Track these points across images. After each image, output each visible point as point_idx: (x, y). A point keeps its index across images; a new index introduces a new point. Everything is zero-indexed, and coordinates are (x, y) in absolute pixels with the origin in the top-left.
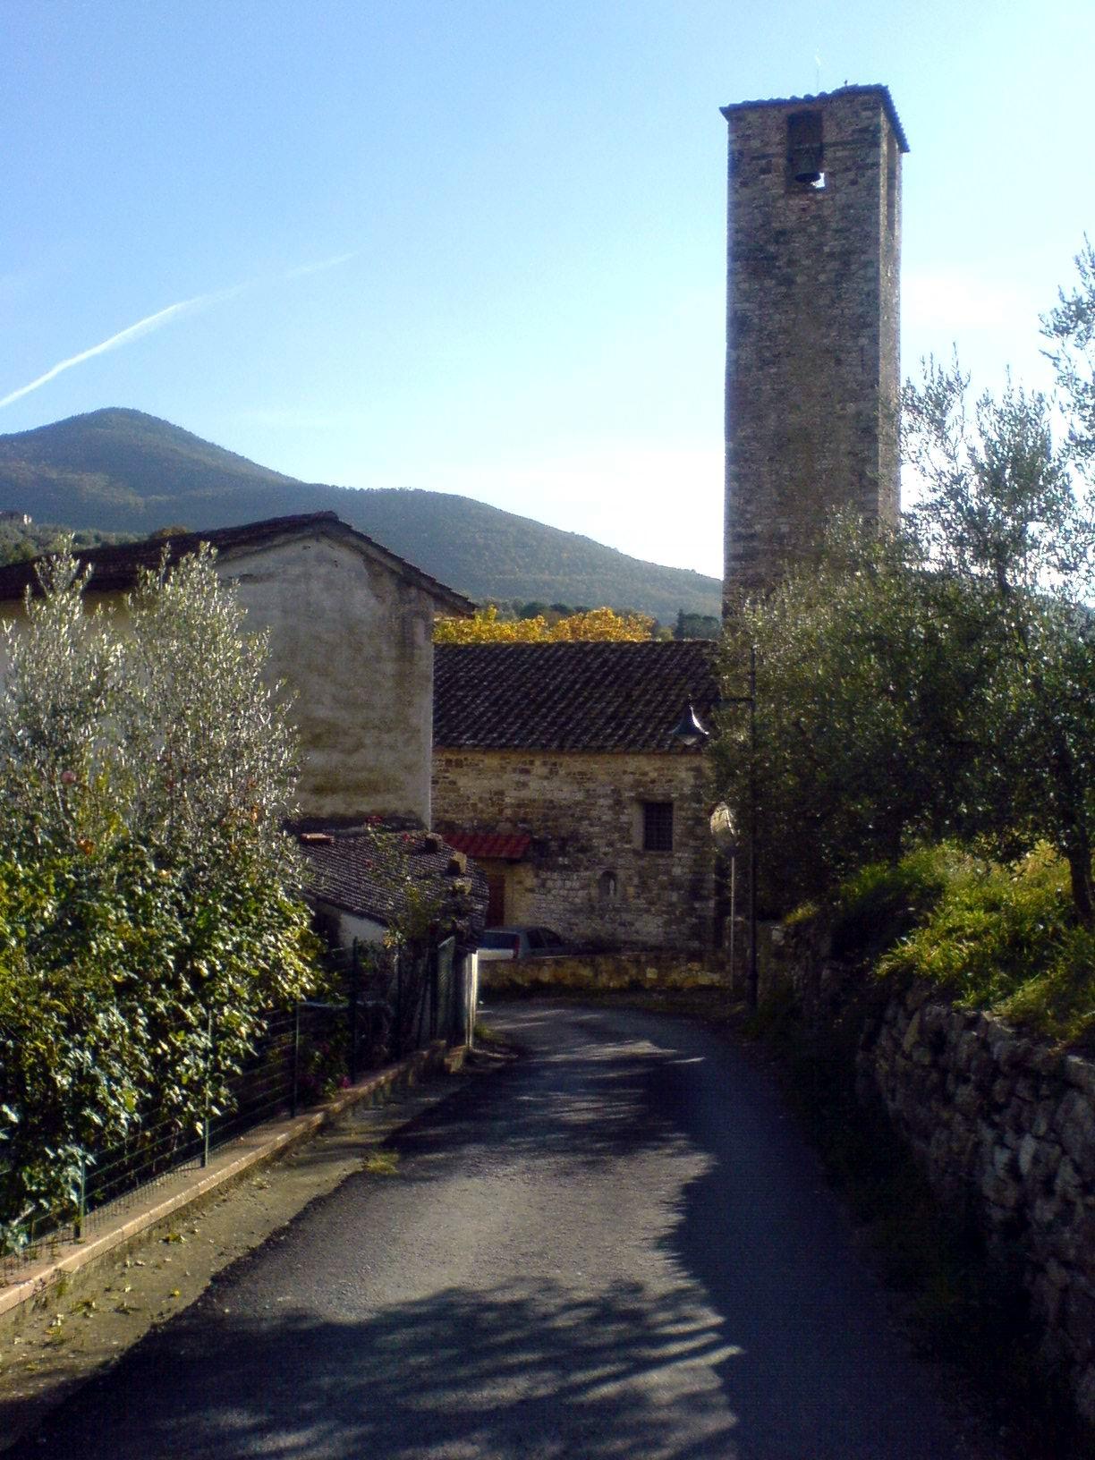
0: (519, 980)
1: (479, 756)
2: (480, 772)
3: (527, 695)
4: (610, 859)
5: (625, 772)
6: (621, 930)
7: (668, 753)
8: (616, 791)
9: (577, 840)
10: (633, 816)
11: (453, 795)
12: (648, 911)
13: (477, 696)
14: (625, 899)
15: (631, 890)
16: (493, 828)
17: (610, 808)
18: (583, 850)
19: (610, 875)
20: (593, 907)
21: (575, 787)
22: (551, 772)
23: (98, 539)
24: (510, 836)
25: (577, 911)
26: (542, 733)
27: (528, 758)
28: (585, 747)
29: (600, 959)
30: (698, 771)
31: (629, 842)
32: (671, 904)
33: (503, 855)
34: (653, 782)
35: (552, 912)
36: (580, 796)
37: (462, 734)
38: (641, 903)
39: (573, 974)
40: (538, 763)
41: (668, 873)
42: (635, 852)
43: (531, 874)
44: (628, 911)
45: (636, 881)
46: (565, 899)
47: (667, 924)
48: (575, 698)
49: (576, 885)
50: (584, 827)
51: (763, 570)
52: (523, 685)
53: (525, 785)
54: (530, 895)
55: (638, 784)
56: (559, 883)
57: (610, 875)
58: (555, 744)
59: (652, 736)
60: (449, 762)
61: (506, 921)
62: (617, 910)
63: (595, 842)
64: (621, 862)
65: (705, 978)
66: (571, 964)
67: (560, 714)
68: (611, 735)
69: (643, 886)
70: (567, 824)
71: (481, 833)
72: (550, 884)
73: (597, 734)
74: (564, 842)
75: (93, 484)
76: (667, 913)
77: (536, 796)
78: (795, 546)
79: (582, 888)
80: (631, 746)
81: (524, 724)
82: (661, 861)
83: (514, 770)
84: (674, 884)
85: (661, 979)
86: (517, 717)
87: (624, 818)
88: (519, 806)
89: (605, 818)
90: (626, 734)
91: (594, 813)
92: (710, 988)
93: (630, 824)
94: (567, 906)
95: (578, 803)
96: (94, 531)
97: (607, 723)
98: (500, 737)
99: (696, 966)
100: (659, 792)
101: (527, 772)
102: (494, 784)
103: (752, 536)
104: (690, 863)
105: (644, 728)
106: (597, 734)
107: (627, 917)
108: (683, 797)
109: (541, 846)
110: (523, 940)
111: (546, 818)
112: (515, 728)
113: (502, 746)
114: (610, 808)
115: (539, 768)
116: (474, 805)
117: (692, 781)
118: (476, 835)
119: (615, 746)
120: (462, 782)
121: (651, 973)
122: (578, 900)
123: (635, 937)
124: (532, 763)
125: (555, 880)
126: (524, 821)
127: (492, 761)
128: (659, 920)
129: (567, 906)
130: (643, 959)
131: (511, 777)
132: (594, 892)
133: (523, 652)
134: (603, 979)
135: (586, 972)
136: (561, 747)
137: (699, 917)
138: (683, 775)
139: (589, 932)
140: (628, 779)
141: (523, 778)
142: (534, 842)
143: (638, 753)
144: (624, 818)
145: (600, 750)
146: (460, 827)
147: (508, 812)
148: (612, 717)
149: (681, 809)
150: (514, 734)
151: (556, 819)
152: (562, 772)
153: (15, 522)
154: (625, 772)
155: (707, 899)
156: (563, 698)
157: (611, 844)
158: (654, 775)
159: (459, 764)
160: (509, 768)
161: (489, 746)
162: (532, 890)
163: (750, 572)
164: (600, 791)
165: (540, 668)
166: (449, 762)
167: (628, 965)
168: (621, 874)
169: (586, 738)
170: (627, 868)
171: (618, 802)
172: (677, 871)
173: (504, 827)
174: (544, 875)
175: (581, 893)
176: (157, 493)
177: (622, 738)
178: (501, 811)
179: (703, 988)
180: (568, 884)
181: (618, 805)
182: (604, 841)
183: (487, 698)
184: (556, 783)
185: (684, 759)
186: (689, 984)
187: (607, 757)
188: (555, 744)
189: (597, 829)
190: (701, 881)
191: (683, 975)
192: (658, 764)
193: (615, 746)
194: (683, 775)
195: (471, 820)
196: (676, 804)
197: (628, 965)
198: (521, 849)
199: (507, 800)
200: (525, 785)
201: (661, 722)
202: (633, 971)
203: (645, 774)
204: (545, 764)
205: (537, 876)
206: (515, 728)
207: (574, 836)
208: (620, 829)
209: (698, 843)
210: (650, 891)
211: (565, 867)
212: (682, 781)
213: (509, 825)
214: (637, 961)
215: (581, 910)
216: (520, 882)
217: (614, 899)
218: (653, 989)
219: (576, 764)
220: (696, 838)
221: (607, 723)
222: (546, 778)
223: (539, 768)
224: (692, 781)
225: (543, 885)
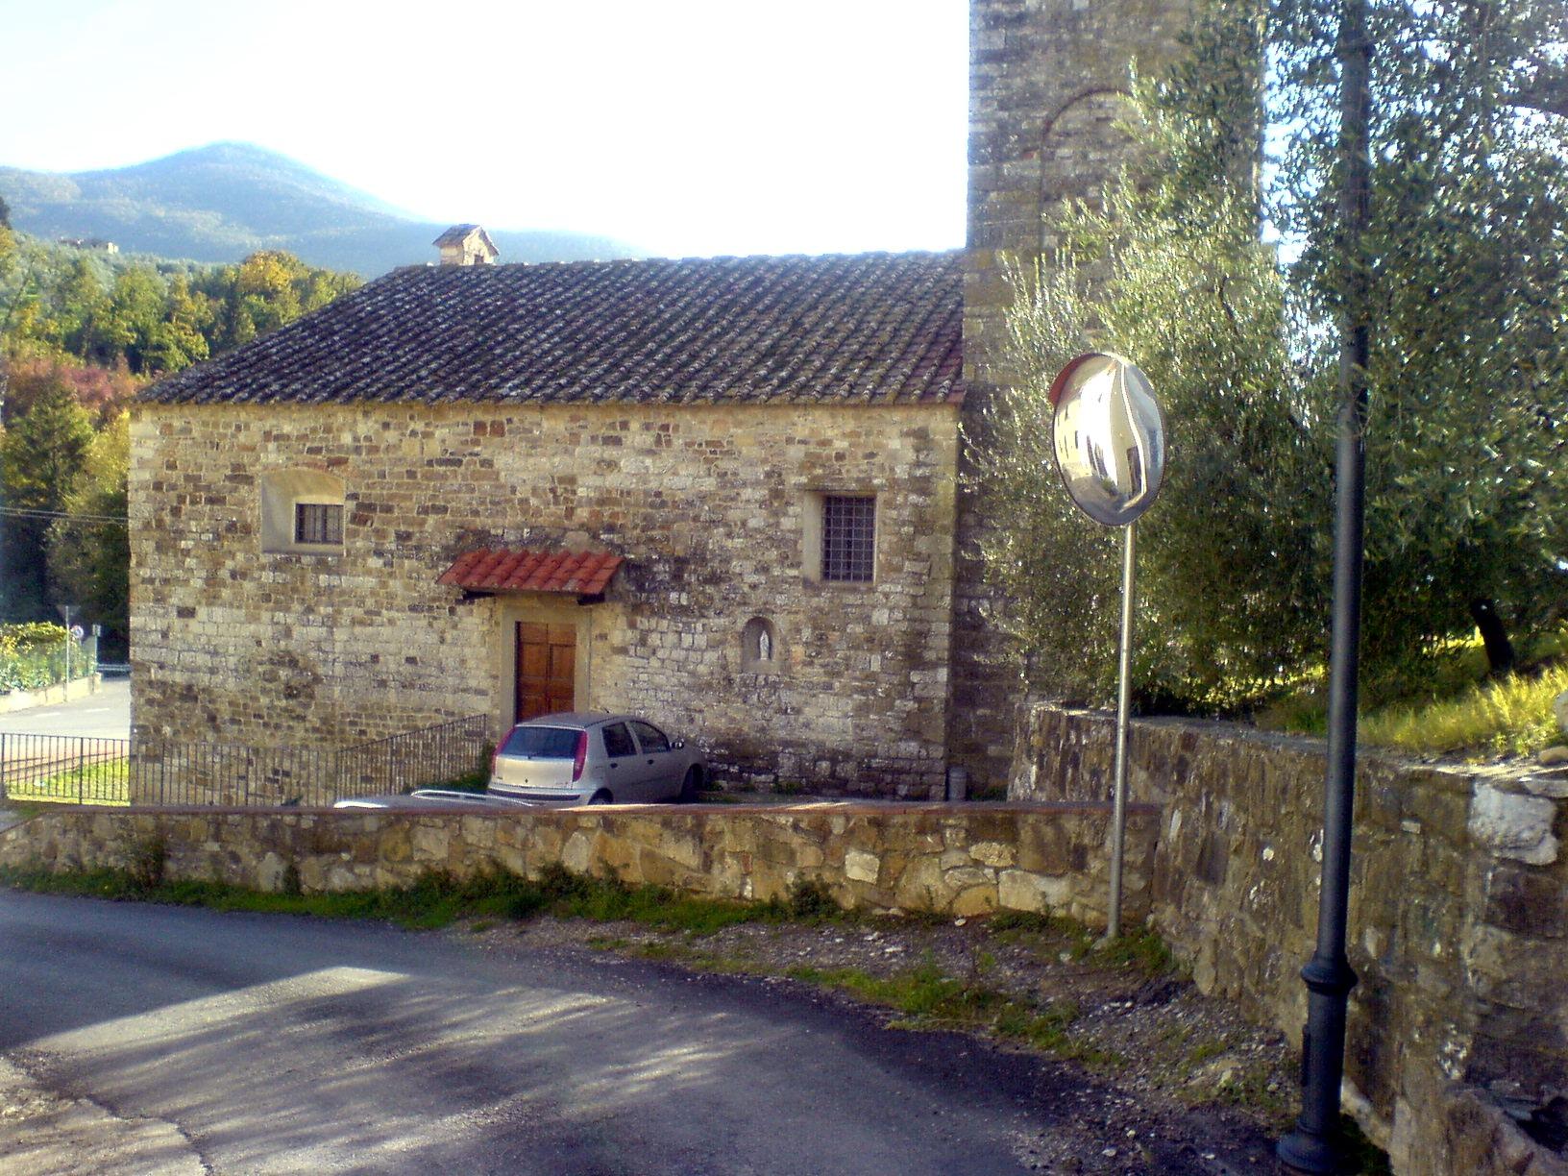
0: (515, 864)
1: (532, 416)
2: (534, 444)
3: (624, 326)
4: (757, 598)
5: (790, 441)
6: (778, 720)
7: (869, 404)
8: (775, 474)
9: (704, 561)
10: (805, 520)
11: (487, 486)
12: (828, 687)
13: (541, 330)
14: (786, 667)
15: (798, 651)
16: (557, 542)
17: (762, 504)
18: (714, 579)
19: (760, 623)
20: (730, 681)
21: (703, 469)
22: (658, 441)
23: (191, 269)
24: (587, 556)
25: (701, 688)
26: (645, 377)
27: (619, 418)
28: (719, 397)
29: (717, 819)
30: (922, 438)
31: (797, 565)
32: (871, 676)
33: (569, 587)
34: (840, 457)
35: (657, 688)
36: (709, 484)
37: (506, 380)
38: (816, 675)
39: (648, 856)
40: (634, 426)
41: (866, 619)
42: (807, 583)
43: (622, 621)
44: (789, 686)
45: (807, 634)
46: (681, 666)
47: (862, 710)
48: (705, 328)
49: (701, 640)
50: (716, 538)
51: (1039, 78)
52: (623, 312)
53: (612, 465)
54: (619, 659)
55: (810, 462)
56: (671, 638)
57: (760, 623)
58: (664, 395)
59: (839, 379)
60: (480, 427)
61: (579, 705)
62: (774, 687)
63: (735, 566)
64: (780, 600)
65: (1025, 892)
66: (639, 827)
67: (679, 350)
68: (766, 379)
69: (821, 641)
70: (684, 536)
71: (535, 550)
72: (654, 639)
73: (740, 379)
74: (680, 564)
75: (205, 223)
76: (862, 691)
77: (631, 484)
78: (1099, 33)
79: (712, 646)
80: (799, 395)
81: (616, 365)
82: (850, 599)
83: (594, 439)
84: (874, 640)
85: (888, 881)
86: (604, 356)
87: (787, 523)
88: (602, 502)
89: (752, 523)
90: (791, 377)
91: (734, 515)
92: (1041, 923)
93: (799, 532)
94: (685, 678)
95: (703, 498)
96: (187, 261)
97: (759, 362)
98: (571, 383)
99: (992, 852)
100: (849, 478)
101: (617, 441)
102: (559, 463)
103: (1020, 19)
104: (905, 602)
105: (824, 368)
106: (740, 379)
107: (787, 697)
108: (894, 484)
109: (638, 572)
110: (594, 741)
111: (649, 523)
112: (599, 370)
113: (573, 397)
114: (762, 504)
115: (637, 435)
116: (524, 501)
117: (911, 456)
118: (526, 554)
119: (773, 394)
120: (501, 461)
121: (859, 867)
122: (701, 669)
123: (805, 735)
124: (625, 426)
125: (663, 632)
126: (610, 529)
127: (554, 424)
128: (849, 706)
129: (685, 678)
130: (838, 826)
131: (588, 451)
132: (733, 653)
133: (627, 271)
134: (726, 878)
135: (683, 854)
136: (676, 398)
137: (918, 700)
138: (895, 444)
139: (722, 724)
140: (796, 452)
141: (610, 452)
142: (629, 566)
143: (817, 404)
144: (787, 523)
145: (747, 400)
146: (499, 539)
147: (583, 514)
148: (771, 352)
149: (889, 504)
150: (598, 378)
151: (666, 525)
152: (678, 442)
153: (98, 250)
154: (790, 441)
155: (934, 665)
156: (683, 329)
157: (764, 569)
158: (841, 445)
159: (498, 430)
160: (585, 436)
161: (550, 398)
162: (623, 651)
163: (1018, 82)
164: (745, 473)
165: (649, 293)
166: (480, 427)
167: (796, 841)
168: (781, 622)
169: (720, 385)
170: (790, 609)
171: (776, 494)
172: (881, 617)
173: (575, 541)
174: (643, 623)
175: (711, 656)
176: (276, 233)
177: (783, 383)
178: (570, 513)
179: (1016, 921)
180: (687, 639)
181: (777, 496)
182: (749, 566)
183: (558, 331)
184: (667, 459)
185: (897, 416)
186: (970, 904)
187: (759, 414)
188: (664, 395)
189: (738, 542)
190: (923, 634)
191: (955, 879)
192: (850, 425)
193: (773, 394)
194: (895, 444)
195: (519, 528)
196: (881, 497)
197: (796, 841)
198: (605, 575)
199: (581, 492)
200: (612, 465)
201: (854, 358)
202: (809, 857)
203: (825, 443)
204: (647, 427)
205: (632, 625)
206: (599, 370)
207: (699, 555)
208: (775, 542)
209: (918, 567)
210: (833, 652)
211: (683, 610)
212: (893, 456)
213: (584, 536)
214: (820, 831)
215: (709, 685)
216: (603, 637)
217: (767, 665)
218: (859, 913)
219: (702, 426)
220: (918, 557)
221: (759, 362)
222: (650, 452)
223: (637, 435)
224: (911, 456)
225: (643, 642)
